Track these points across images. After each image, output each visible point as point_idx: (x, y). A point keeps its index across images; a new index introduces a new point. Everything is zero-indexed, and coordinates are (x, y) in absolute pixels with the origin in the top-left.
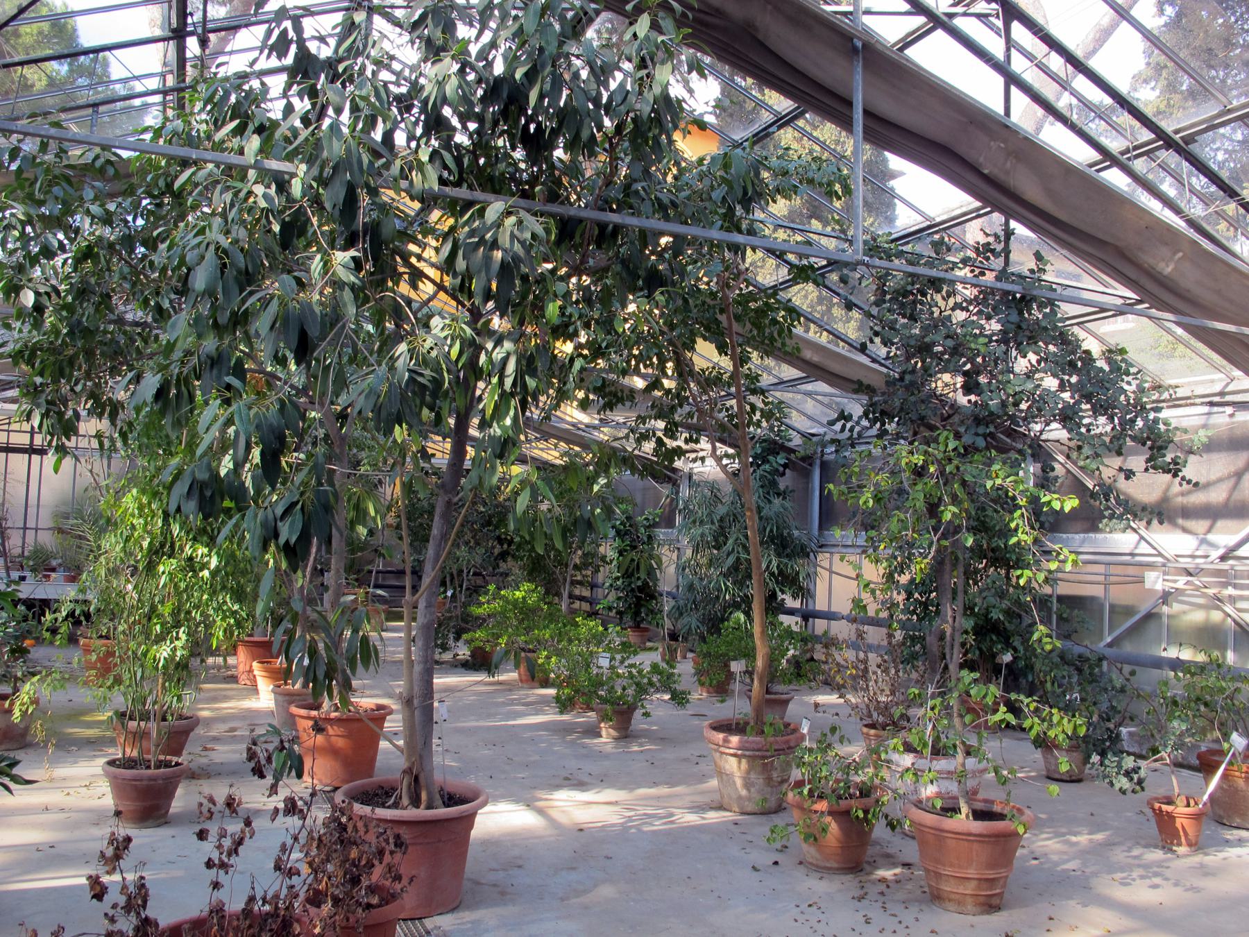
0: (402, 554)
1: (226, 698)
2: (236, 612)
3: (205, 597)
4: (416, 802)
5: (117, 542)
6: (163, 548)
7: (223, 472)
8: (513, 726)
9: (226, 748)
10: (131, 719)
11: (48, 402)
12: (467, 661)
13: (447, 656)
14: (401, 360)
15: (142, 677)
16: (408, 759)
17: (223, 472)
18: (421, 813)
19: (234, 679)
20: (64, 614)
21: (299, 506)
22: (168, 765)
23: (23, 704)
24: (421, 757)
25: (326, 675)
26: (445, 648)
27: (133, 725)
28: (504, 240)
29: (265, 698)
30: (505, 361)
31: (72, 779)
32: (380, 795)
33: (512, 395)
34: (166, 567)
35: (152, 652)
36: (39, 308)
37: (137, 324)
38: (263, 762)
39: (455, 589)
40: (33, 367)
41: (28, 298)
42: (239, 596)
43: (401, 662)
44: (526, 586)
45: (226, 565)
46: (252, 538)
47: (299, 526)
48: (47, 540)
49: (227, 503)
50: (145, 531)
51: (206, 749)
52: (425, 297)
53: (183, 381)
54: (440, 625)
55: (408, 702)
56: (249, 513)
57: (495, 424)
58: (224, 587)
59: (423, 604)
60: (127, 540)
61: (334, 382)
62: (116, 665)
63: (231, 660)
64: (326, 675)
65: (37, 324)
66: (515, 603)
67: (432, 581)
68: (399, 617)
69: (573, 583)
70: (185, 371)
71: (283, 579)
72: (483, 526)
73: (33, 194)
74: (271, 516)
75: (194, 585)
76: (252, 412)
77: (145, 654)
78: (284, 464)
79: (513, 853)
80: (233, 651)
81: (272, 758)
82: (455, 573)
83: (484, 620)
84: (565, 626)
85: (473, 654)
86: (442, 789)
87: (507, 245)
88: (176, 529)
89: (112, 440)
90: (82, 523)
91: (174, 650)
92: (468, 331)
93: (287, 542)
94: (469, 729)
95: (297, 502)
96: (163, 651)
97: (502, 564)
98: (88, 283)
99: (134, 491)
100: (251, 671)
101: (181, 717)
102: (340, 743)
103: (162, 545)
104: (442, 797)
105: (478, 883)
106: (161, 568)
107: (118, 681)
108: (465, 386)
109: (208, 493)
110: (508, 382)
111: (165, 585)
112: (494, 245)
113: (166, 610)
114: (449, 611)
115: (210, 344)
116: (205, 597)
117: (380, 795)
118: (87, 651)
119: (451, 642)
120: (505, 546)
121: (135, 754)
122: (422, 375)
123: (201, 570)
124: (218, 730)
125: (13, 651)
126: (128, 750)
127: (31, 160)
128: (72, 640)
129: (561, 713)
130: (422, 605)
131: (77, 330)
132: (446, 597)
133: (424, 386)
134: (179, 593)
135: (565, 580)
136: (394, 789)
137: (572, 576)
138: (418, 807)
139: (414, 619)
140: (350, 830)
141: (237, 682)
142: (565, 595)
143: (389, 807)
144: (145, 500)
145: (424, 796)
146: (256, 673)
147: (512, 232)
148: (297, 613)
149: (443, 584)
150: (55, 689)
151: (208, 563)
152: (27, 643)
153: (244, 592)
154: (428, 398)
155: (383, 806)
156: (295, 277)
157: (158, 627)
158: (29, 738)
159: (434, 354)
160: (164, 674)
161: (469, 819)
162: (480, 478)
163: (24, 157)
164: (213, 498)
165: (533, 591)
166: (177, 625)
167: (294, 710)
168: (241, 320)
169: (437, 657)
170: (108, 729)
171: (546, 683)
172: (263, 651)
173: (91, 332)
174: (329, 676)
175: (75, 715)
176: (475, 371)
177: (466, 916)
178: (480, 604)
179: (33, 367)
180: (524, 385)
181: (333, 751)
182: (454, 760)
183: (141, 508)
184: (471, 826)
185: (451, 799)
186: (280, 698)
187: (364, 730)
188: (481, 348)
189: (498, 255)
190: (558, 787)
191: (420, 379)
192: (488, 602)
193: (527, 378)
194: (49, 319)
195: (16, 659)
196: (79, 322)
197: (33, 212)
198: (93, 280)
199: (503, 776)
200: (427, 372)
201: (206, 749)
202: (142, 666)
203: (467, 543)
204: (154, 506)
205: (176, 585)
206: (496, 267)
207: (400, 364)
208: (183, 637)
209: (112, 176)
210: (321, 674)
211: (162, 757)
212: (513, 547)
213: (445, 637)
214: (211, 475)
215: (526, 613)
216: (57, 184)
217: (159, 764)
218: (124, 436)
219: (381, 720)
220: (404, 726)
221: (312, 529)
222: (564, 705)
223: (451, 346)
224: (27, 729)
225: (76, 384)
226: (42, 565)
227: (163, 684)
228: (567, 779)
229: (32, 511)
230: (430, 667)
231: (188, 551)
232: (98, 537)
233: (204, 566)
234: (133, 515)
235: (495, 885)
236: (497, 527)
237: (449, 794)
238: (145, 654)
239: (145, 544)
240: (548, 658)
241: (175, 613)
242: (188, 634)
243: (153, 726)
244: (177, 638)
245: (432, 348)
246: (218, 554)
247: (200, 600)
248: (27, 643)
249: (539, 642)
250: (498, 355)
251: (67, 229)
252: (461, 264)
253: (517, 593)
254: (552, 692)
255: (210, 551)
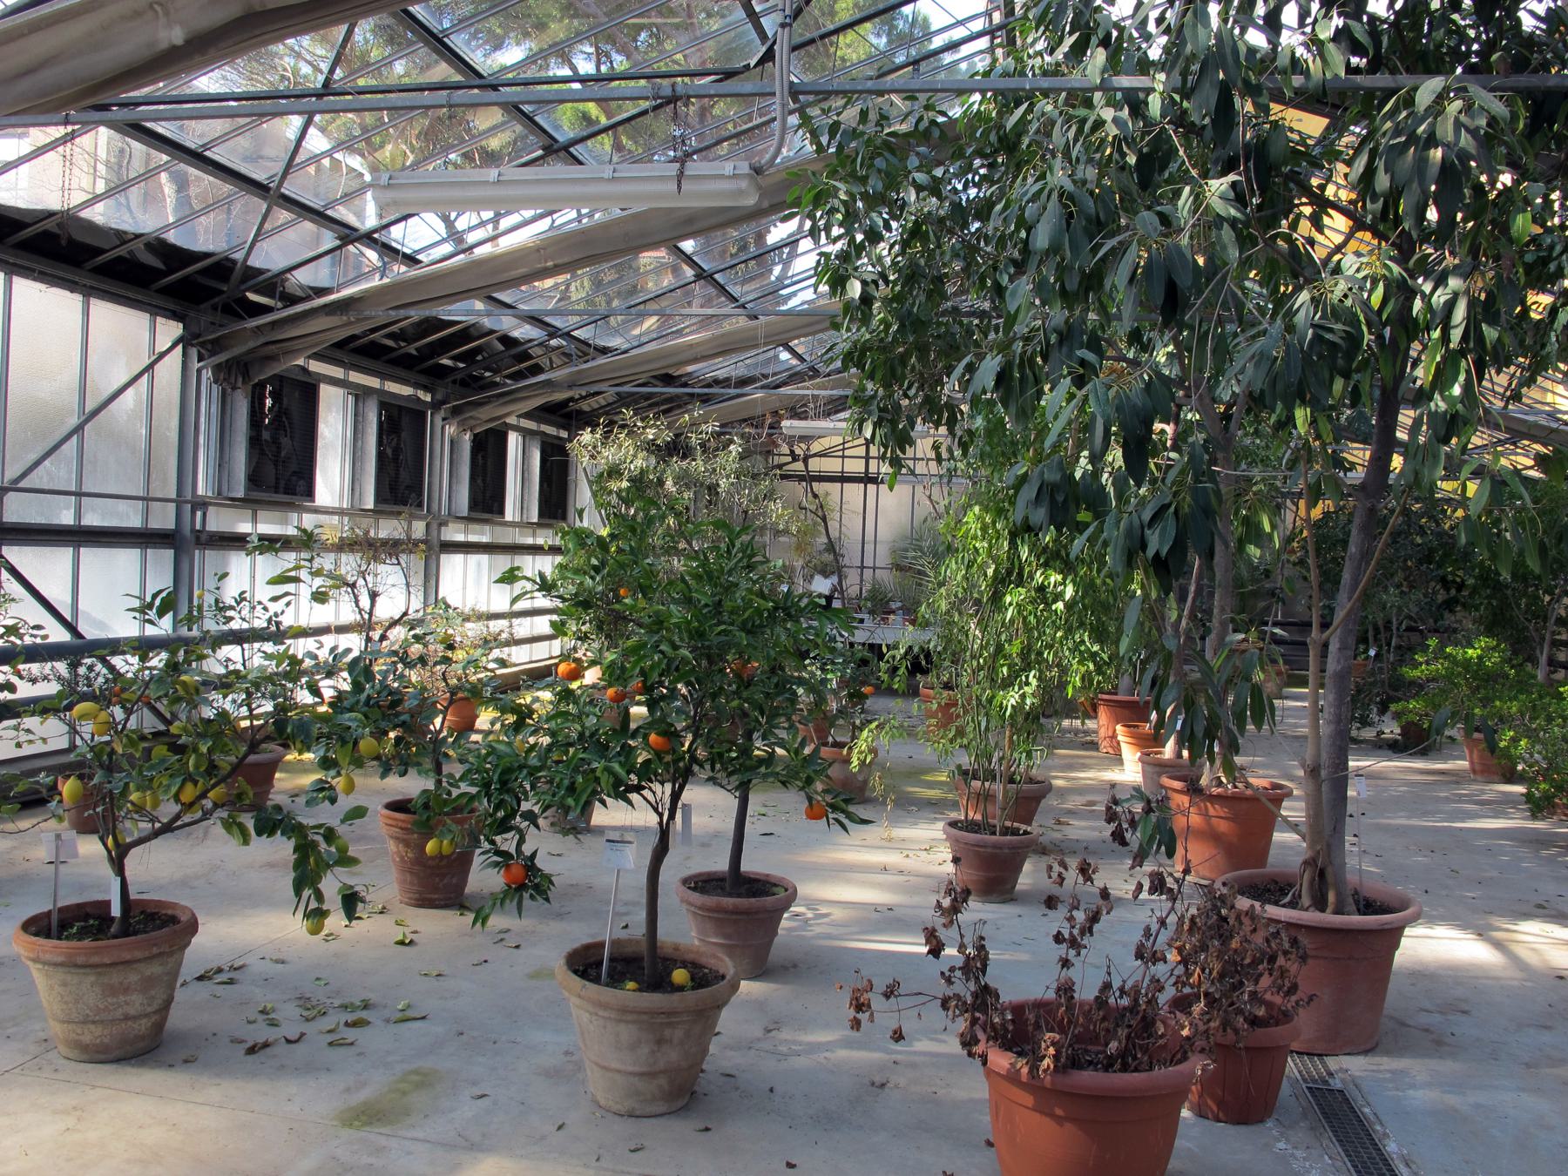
0: (1308, 605)
1: (1084, 767)
2: (1095, 654)
3: (1059, 634)
4: (1320, 904)
5: (958, 569)
6: (1011, 575)
7: (1078, 475)
8: (1461, 829)
9: (1083, 824)
10: (975, 778)
11: (880, 410)
12: (1396, 741)
13: (1369, 734)
14: (1302, 313)
15: (987, 728)
16: (1311, 846)
17: (1078, 475)
18: (1329, 918)
19: (1094, 746)
20: (902, 651)
21: (1172, 509)
22: (1015, 832)
23: (861, 752)
24: (1329, 846)
25: (1209, 732)
26: (1365, 722)
27: (976, 784)
28: (1446, 130)
29: (1130, 771)
30: (1450, 306)
31: (912, 841)
32: (1274, 889)
33: (1462, 353)
34: (1014, 597)
35: (999, 698)
36: (866, 300)
37: (972, 314)
38: (1125, 826)
39: (1380, 647)
40: (863, 370)
41: (855, 289)
42: (1100, 635)
43: (1305, 737)
44: (1484, 641)
45: (1083, 597)
46: (1114, 559)
47: (1172, 533)
48: (886, 578)
49: (1083, 516)
50: (989, 554)
51: (1059, 823)
52: (1339, 239)
53: (1027, 362)
54: (1359, 691)
55: (1313, 772)
56: (1110, 520)
57: (1437, 396)
58: (1082, 625)
59: (1334, 647)
60: (969, 567)
61: (1214, 351)
62: (958, 716)
63: (1090, 724)
64: (1209, 732)
65: (866, 319)
66: (1467, 663)
67: (1348, 615)
68: (1303, 682)
69: (1555, 644)
70: (1029, 349)
71: (1153, 614)
72: (1420, 562)
73: (855, 170)
74: (1136, 522)
75: (1046, 619)
76: (1112, 393)
77: (990, 701)
78: (1152, 466)
79: (1452, 992)
80: (1091, 712)
81: (1142, 827)
82: (1380, 623)
83: (1421, 687)
84: (1541, 697)
85: (1405, 731)
86: (1356, 893)
87: (1450, 137)
88: (1024, 553)
89: (950, 450)
90: (920, 555)
91: (1023, 696)
92: (1396, 269)
93: (1157, 553)
94: (1398, 828)
95: (1169, 505)
96: (1011, 699)
97: (1447, 615)
98: (918, 265)
99: (977, 509)
100: (1114, 736)
101: (1031, 781)
102: (1223, 826)
103: (1009, 572)
104: (1357, 902)
105: (1403, 1024)
106: (1008, 599)
107: (961, 733)
108: (1395, 353)
109: (1060, 498)
110: (1456, 335)
111: (1012, 621)
112: (1431, 140)
113: (1014, 649)
114: (1372, 673)
115: (1058, 315)
116: (1059, 634)
117: (1274, 889)
118: (928, 699)
119: (1374, 716)
120: (1453, 592)
121: (978, 817)
122: (1331, 330)
123: (1055, 601)
124: (1074, 802)
125: (851, 696)
126: (971, 814)
127: (854, 134)
128: (912, 692)
129: (1534, 817)
130: (1334, 647)
131: (911, 323)
132: (1368, 657)
133: (1333, 344)
134: (1028, 629)
135: (1543, 639)
136: (1291, 886)
137: (1553, 633)
138: (1323, 911)
139: (1322, 686)
140: (1231, 921)
141: (1097, 749)
142: (1543, 659)
143: (1284, 906)
144: (988, 519)
145: (1331, 897)
146: (1120, 738)
147: (1457, 120)
148: (1170, 653)
149: (1363, 640)
150: (893, 737)
151: (1062, 594)
152: (866, 690)
153: (1105, 630)
154: (1340, 362)
155: (1276, 903)
156: (1160, 214)
157: (1005, 670)
158: (867, 794)
159: (1349, 302)
160: (1012, 726)
161: (1393, 936)
162: (1416, 474)
163: (845, 131)
164: (1067, 501)
165: (1494, 649)
166: (1027, 667)
167: (1166, 781)
168: (1093, 281)
169: (1354, 733)
170: (950, 791)
171: (1511, 777)
172: (1131, 713)
173: (923, 323)
174: (1210, 735)
175: (915, 773)
176: (1408, 328)
177: (1386, 1063)
178: (1416, 665)
179: (863, 370)
180: (1480, 338)
181: (1212, 836)
182: (1375, 866)
183: (984, 529)
184: (1396, 945)
185: (1368, 906)
186: (1149, 769)
187: (1254, 815)
188: (1411, 293)
189: (1437, 154)
190: (1527, 916)
191: (1328, 336)
192: (1427, 663)
193: (1484, 326)
194: (878, 312)
195: (854, 706)
196: (910, 313)
197: (855, 190)
198: (922, 262)
199: (1444, 893)
200: (1339, 327)
201: (1059, 823)
202: (987, 714)
203: (1398, 586)
204: (999, 526)
205: (1025, 618)
206: (1434, 171)
207: (1300, 318)
208: (1034, 682)
209: (944, 141)
210: (1199, 730)
211: (1008, 824)
212: (1465, 593)
213: (1366, 707)
214: (1064, 475)
215: (1483, 680)
216: (880, 155)
217: (1006, 831)
218: (964, 447)
219: (1278, 801)
220: (1308, 816)
221: (1186, 541)
222: (1538, 806)
223: (1371, 292)
224: (866, 782)
225: (909, 388)
226: (880, 605)
227: (1011, 738)
228: (1540, 906)
229: (869, 548)
230: (1343, 744)
231: (1039, 577)
232: (936, 568)
233: (1058, 597)
234: (975, 537)
235: (1427, 1030)
236: (1440, 566)
237: (1366, 900)
238: (990, 701)
239: (990, 572)
240: (1515, 740)
241: (1025, 653)
242: (1040, 679)
243: (998, 788)
244: (1027, 684)
245: (1346, 296)
246: (1073, 581)
247: (1053, 639)
248: (866, 690)
249: (1501, 720)
250: (1440, 298)
251: (891, 204)
252: (1382, 181)
253: (1470, 651)
254: (1520, 789)
255: (1064, 579)
